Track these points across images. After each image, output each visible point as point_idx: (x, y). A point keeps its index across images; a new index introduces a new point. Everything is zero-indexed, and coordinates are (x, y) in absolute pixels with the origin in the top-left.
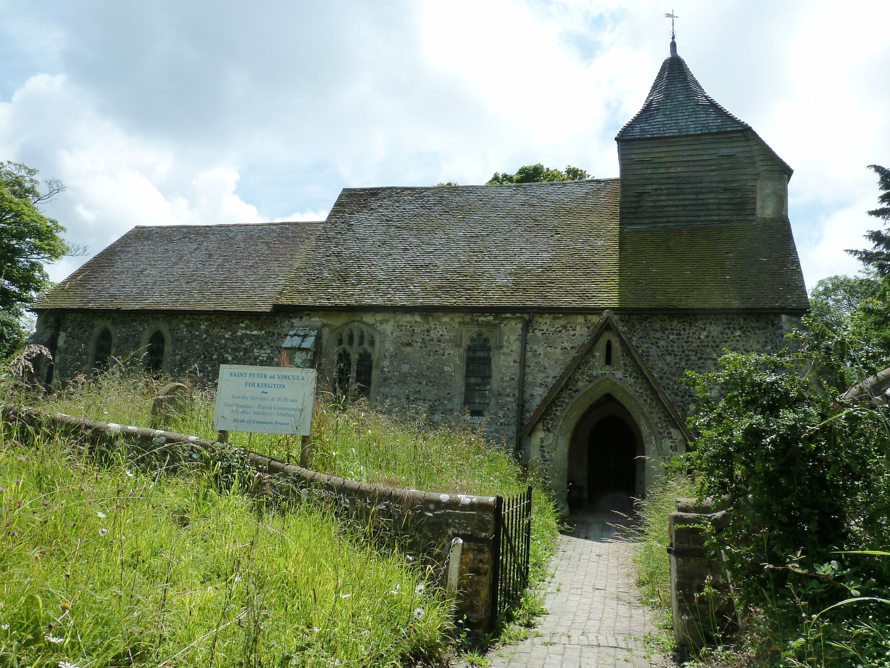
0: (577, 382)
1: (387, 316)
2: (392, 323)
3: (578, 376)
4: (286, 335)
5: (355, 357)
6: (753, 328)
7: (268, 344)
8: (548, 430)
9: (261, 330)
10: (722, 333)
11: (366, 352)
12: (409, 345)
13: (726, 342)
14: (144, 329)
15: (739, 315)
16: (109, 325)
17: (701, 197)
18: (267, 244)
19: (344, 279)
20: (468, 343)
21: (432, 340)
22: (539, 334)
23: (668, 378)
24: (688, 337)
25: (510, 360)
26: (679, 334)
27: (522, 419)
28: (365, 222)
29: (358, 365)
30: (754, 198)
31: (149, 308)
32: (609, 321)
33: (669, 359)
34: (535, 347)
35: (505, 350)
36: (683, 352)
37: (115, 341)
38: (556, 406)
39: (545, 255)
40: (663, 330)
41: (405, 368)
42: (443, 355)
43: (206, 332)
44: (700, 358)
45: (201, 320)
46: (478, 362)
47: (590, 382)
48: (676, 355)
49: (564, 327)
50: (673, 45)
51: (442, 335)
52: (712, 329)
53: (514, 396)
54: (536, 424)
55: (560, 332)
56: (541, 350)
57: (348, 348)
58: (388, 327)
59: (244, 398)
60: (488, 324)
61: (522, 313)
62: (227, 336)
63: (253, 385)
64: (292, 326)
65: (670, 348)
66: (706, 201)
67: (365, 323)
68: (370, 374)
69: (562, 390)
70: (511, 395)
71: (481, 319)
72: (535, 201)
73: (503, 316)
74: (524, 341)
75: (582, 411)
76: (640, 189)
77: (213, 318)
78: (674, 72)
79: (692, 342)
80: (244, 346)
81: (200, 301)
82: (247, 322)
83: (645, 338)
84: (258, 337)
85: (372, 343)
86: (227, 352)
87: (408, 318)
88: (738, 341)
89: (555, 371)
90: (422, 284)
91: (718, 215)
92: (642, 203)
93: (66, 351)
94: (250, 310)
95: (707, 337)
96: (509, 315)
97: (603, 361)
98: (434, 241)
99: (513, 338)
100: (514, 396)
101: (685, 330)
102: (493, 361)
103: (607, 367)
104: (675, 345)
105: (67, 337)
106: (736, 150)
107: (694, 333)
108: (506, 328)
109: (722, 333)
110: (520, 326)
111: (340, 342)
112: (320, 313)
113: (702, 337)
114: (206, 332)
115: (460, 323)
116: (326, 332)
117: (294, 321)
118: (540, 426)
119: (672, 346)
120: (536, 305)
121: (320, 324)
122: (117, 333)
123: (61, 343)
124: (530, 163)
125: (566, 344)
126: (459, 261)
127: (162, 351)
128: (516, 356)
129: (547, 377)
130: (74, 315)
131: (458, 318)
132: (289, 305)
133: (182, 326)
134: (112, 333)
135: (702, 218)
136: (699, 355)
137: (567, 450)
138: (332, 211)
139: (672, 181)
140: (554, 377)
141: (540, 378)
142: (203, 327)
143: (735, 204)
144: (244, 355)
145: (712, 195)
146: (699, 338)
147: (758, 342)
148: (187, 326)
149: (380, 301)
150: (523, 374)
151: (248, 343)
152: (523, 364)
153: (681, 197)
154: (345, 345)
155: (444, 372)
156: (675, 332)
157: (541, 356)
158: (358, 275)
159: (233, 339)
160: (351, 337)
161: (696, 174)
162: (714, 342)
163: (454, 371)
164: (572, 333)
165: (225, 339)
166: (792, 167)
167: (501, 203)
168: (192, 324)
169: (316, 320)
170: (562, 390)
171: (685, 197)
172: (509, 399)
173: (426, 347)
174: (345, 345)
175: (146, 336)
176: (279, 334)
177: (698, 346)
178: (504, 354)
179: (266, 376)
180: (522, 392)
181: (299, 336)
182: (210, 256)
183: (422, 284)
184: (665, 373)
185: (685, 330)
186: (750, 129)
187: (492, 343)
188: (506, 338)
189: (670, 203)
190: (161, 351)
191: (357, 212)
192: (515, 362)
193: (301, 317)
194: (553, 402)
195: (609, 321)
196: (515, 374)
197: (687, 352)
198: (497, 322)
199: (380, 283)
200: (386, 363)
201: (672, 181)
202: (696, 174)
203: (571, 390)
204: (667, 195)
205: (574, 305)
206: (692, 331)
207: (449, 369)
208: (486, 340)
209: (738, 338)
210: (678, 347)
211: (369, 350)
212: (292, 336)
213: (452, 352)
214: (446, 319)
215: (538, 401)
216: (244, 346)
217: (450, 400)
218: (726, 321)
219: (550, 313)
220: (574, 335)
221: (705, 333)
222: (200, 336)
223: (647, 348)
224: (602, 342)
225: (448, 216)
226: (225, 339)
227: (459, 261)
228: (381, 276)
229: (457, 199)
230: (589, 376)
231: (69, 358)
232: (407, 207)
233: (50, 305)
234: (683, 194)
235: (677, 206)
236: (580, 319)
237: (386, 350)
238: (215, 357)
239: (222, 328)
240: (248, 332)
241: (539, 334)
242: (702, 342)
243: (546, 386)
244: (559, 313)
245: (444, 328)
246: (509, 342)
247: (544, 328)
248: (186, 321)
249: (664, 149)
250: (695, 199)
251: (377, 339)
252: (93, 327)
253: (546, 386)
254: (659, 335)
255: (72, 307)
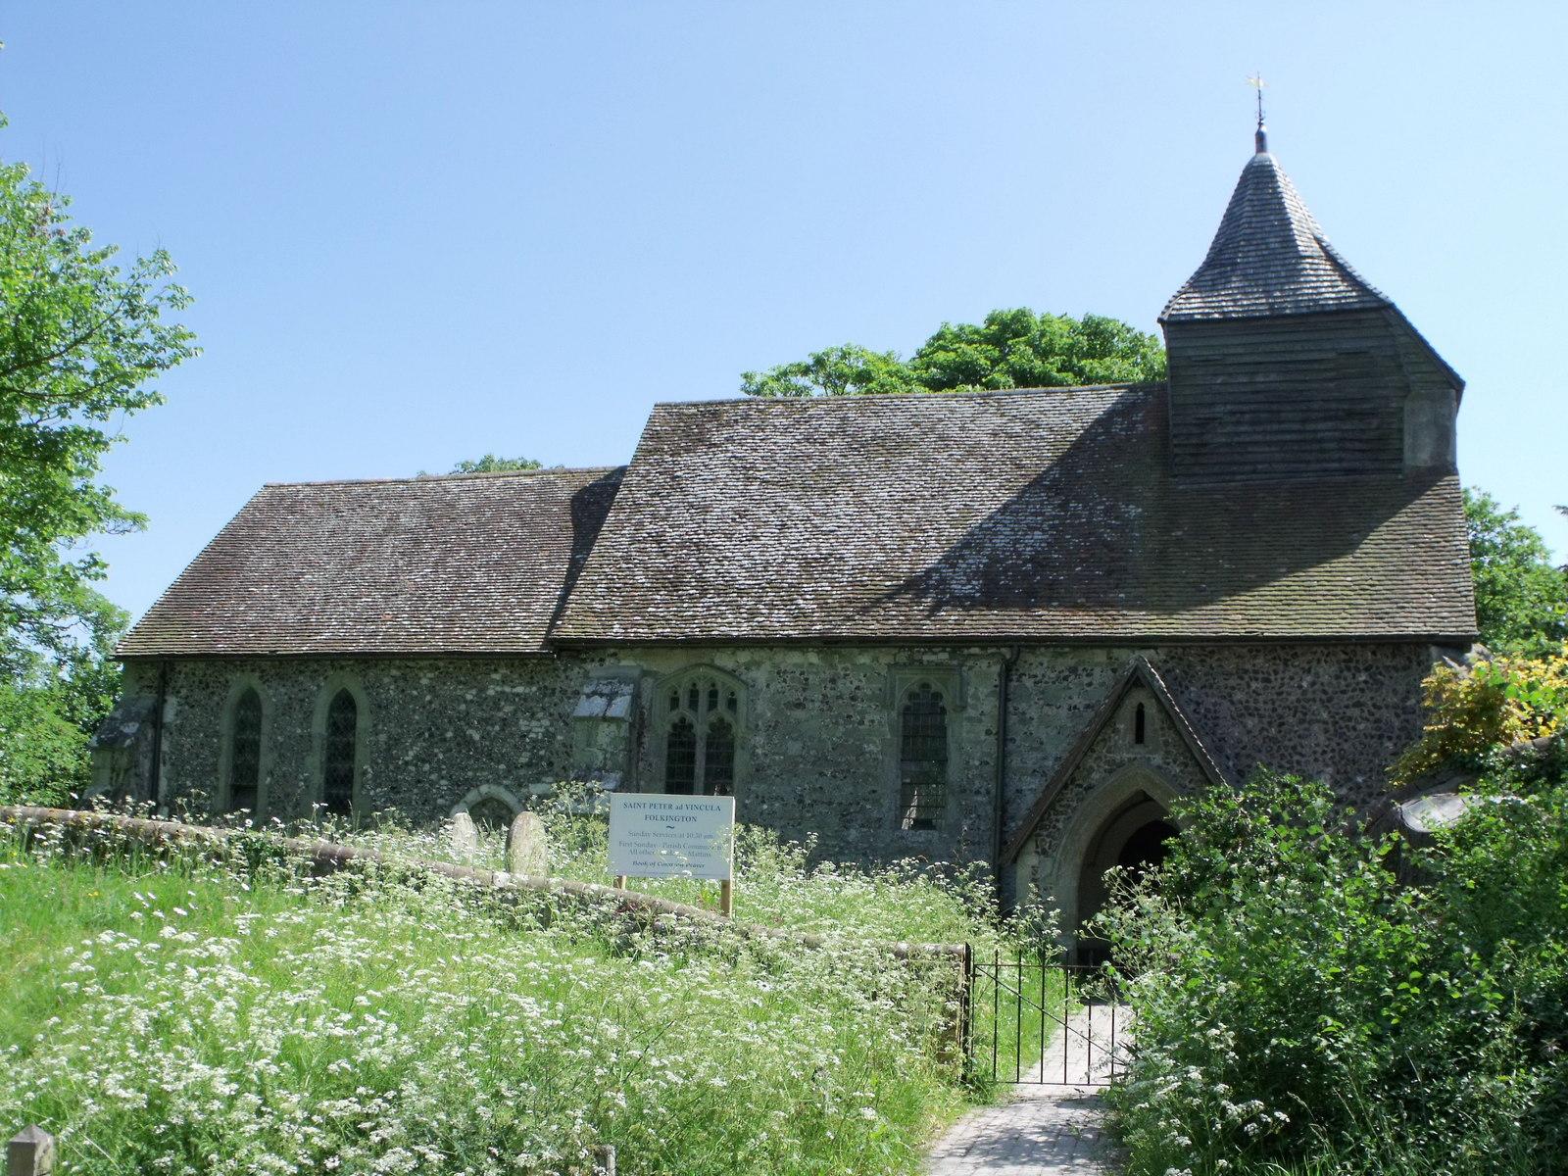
0: (1090, 773)
1: (760, 655)
2: (767, 666)
3: (1090, 762)
4: (577, 693)
5: (701, 730)
6: (1387, 668)
7: (543, 709)
8: (1044, 852)
9: (530, 683)
10: (1337, 677)
11: (721, 720)
12: (799, 705)
13: (1344, 692)
14: (318, 686)
15: (1363, 646)
16: (254, 680)
17: (1311, 427)
18: (520, 516)
19: (675, 585)
20: (906, 702)
21: (840, 697)
22: (1029, 683)
23: (1248, 756)
24: (1282, 685)
25: (981, 728)
26: (1267, 680)
27: (1002, 833)
28: (709, 475)
29: (709, 745)
30: (1401, 430)
31: (326, 650)
32: (1139, 673)
33: (1250, 723)
34: (1023, 706)
35: (971, 713)
36: (1274, 710)
37: (267, 710)
38: (1057, 813)
39: (1038, 535)
40: (1241, 673)
41: (794, 748)
42: (861, 723)
43: (431, 689)
44: (1302, 721)
45: (420, 669)
46: (923, 729)
47: (1110, 772)
48: (1261, 716)
49: (1073, 670)
50: (1261, 138)
51: (858, 688)
52: (1321, 671)
53: (988, 792)
54: (1025, 843)
55: (1066, 678)
56: (1033, 713)
57: (690, 716)
58: (760, 676)
59: (643, 834)
60: (939, 665)
61: (998, 648)
62: (469, 697)
63: (655, 818)
64: (586, 675)
65: (1252, 704)
66: (1319, 435)
67: (719, 669)
68: (730, 758)
69: (1065, 787)
70: (983, 790)
71: (926, 658)
72: (1018, 428)
73: (966, 651)
74: (1004, 697)
75: (1099, 821)
76: (1204, 413)
77: (441, 664)
78: (1257, 209)
79: (1289, 694)
80: (500, 714)
81: (416, 634)
82: (503, 671)
83: (1211, 687)
84: (525, 698)
85: (732, 704)
86: (470, 725)
87: (795, 658)
88: (1362, 690)
89: (1057, 748)
90: (818, 596)
91: (1340, 460)
92: (1207, 438)
93: (180, 729)
94: (509, 649)
95: (1313, 684)
96: (975, 650)
97: (1131, 737)
98: (836, 510)
99: (983, 691)
100: (988, 792)
101: (1276, 672)
102: (949, 733)
103: (1139, 748)
104: (1261, 699)
105: (180, 704)
106: (1370, 343)
107: (1292, 678)
108: (972, 673)
109: (1337, 677)
110: (996, 669)
111: (675, 702)
112: (638, 651)
113: (1305, 684)
114: (431, 689)
115: (889, 666)
116: (648, 684)
117: (589, 666)
118: (1031, 846)
119: (1256, 701)
120: (1022, 633)
121: (636, 673)
122: (271, 696)
123: (169, 715)
124: (1008, 306)
125: (1076, 701)
126: (883, 548)
127: (353, 727)
128: (989, 723)
129: (1045, 759)
130: (191, 665)
131: (885, 658)
132: (579, 640)
133: (386, 680)
134: (262, 696)
135: (1314, 466)
136: (1299, 715)
137: (1075, 884)
138: (639, 449)
139: (1261, 397)
140: (1057, 759)
141: (1032, 759)
142: (424, 681)
143: (1368, 441)
144: (503, 730)
145: (1330, 425)
146: (1300, 687)
147: (1395, 692)
148: (396, 680)
149: (745, 629)
150: (1003, 755)
151: (508, 709)
152: (1003, 736)
153: (1275, 427)
154: (683, 708)
155: (863, 754)
156: (1260, 676)
157: (1034, 723)
158: (700, 579)
159: (481, 701)
160: (694, 694)
161: (1295, 399)
162: (1325, 692)
163: (882, 752)
164: (1086, 680)
165: (465, 702)
166: (1463, 376)
167: (954, 432)
168: (404, 678)
169: (628, 663)
170: (1065, 787)
171: (1284, 426)
172: (979, 798)
173: (830, 709)
174: (683, 708)
175: (322, 702)
176: (563, 692)
177: (1298, 701)
178: (970, 719)
179: (670, 806)
180: (1002, 786)
181: (601, 695)
182: (417, 542)
183: (818, 596)
184: (1244, 748)
185: (1276, 672)
186: (1391, 307)
187: (947, 701)
188: (971, 691)
189: (1259, 438)
190: (351, 726)
191: (687, 451)
192: (988, 732)
193: (602, 660)
194: (1052, 806)
195: (1139, 673)
196: (989, 755)
197: (1280, 711)
198: (955, 662)
199: (741, 593)
200: (760, 740)
201: (1261, 397)
202: (1301, 387)
203: (1080, 786)
204: (1252, 423)
205: (1089, 632)
206: (1287, 675)
207: (872, 747)
208: (938, 696)
209: (1362, 686)
210: (1265, 703)
211: (728, 717)
212: (589, 696)
213: (876, 717)
214: (864, 659)
215: (1030, 799)
216: (500, 714)
217: (876, 802)
218: (1343, 656)
219: (1047, 647)
220: (1090, 684)
221: (1309, 678)
222: (421, 696)
223: (1215, 704)
224: (1128, 711)
225: (859, 459)
226: (465, 702)
227: (883, 548)
228: (742, 580)
229: (874, 423)
230: (1107, 762)
231: (187, 742)
232: (779, 439)
233: (139, 649)
234: (1280, 422)
235: (1269, 444)
236: (1100, 656)
237: (761, 716)
238: (449, 735)
239: (460, 683)
240: (507, 689)
241: (1029, 683)
242: (1304, 692)
243: (1044, 774)
244: (1063, 647)
245: (863, 673)
246: (976, 697)
247: (1038, 672)
248: (394, 672)
249: (1245, 340)
250: (1300, 432)
251: (742, 696)
252: (226, 685)
253: (1044, 774)
254: (1232, 682)
255: (188, 651)
